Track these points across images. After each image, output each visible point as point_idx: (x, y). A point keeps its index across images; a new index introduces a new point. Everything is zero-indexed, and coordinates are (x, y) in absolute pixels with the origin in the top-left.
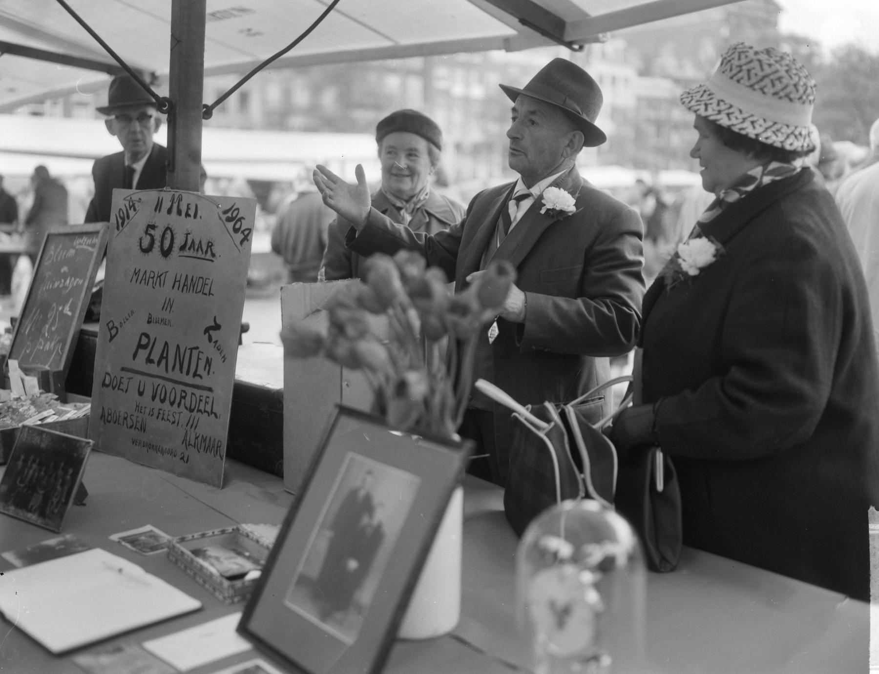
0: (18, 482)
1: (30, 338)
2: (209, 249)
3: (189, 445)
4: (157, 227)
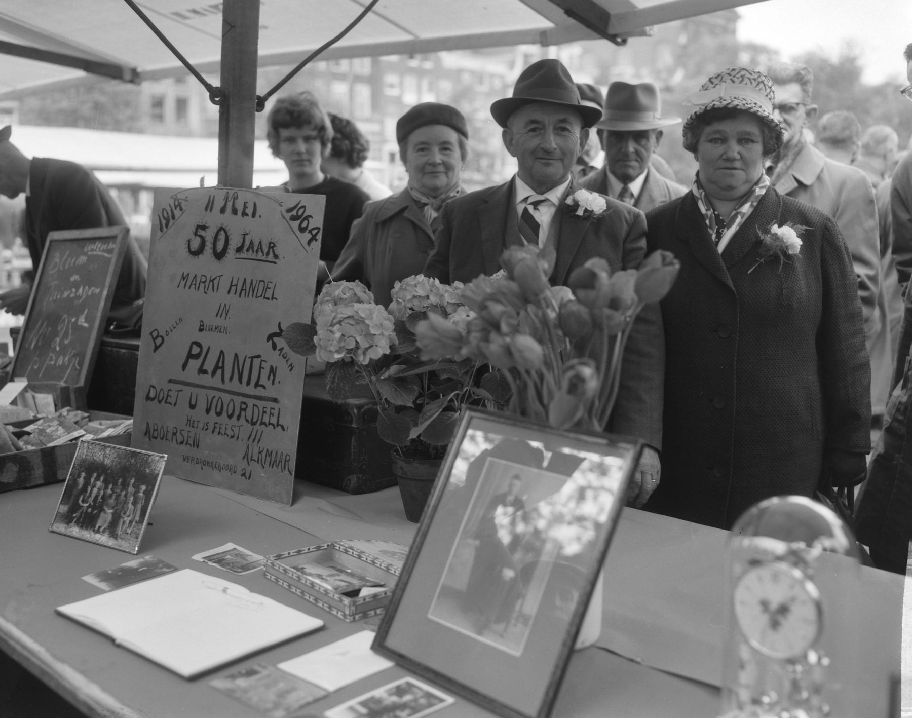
0: (80, 501)
1: (37, 353)
2: (271, 250)
3: (251, 460)
4: (208, 227)
